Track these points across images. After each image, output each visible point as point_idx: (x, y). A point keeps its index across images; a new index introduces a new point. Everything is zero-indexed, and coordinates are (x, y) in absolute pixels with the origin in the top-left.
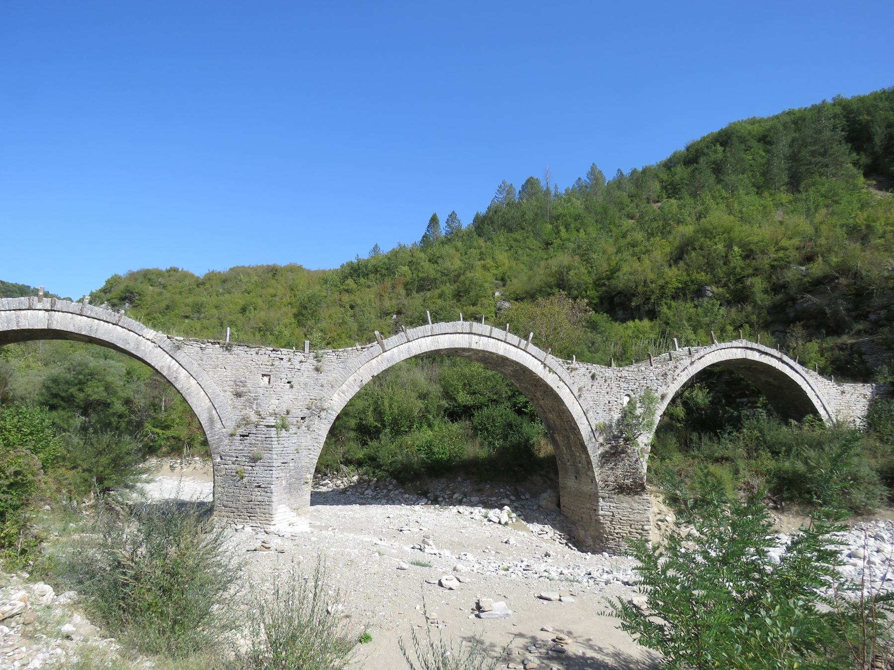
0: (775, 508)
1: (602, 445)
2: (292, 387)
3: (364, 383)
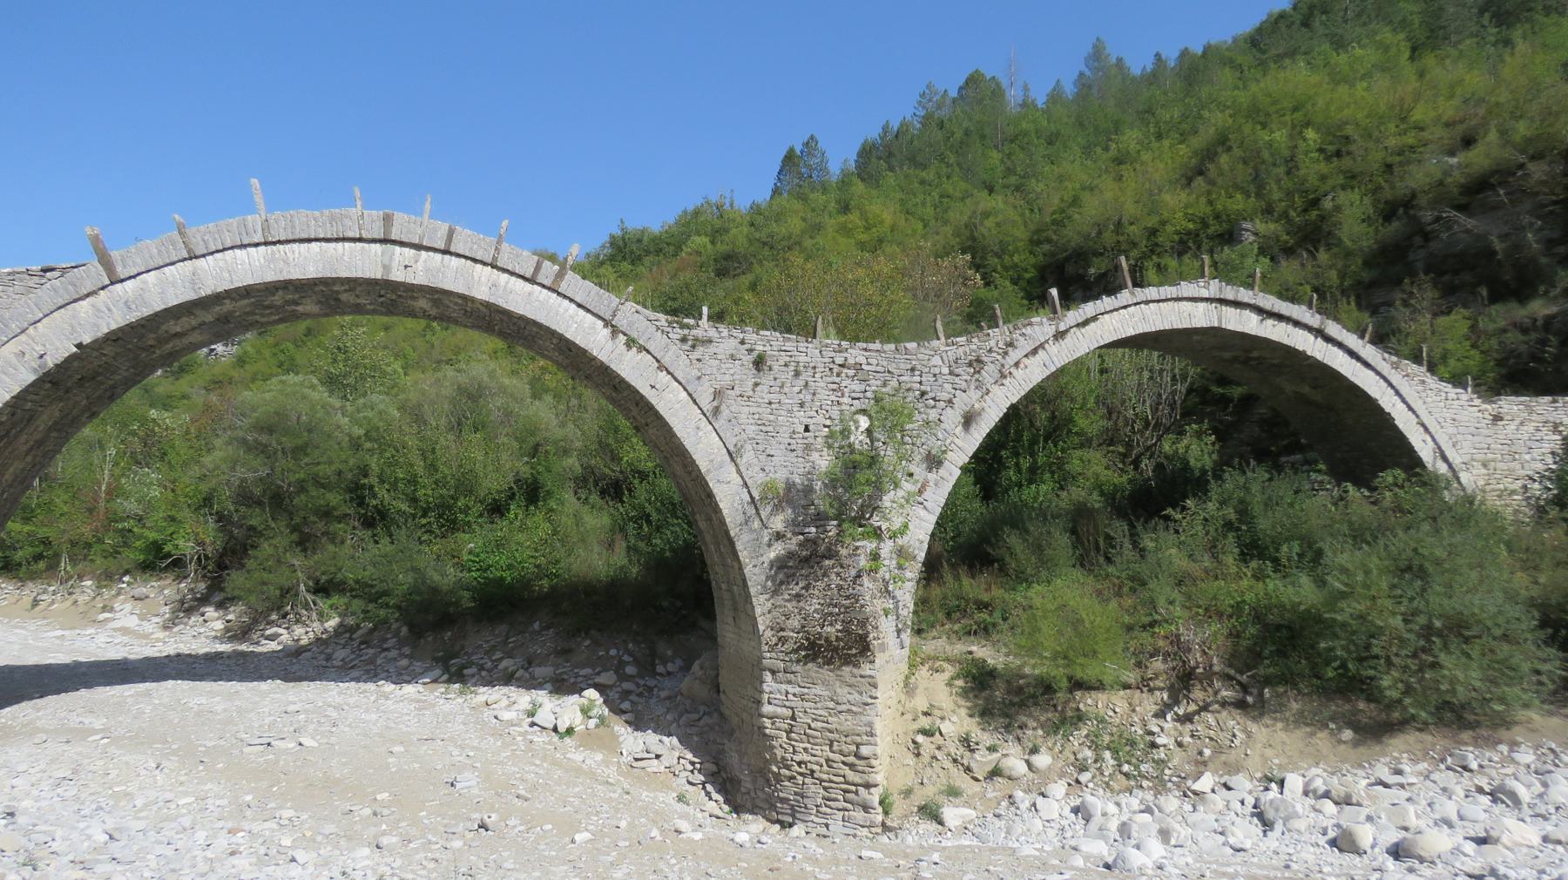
0: (1241, 705)
1: (779, 536)
3: (50, 362)
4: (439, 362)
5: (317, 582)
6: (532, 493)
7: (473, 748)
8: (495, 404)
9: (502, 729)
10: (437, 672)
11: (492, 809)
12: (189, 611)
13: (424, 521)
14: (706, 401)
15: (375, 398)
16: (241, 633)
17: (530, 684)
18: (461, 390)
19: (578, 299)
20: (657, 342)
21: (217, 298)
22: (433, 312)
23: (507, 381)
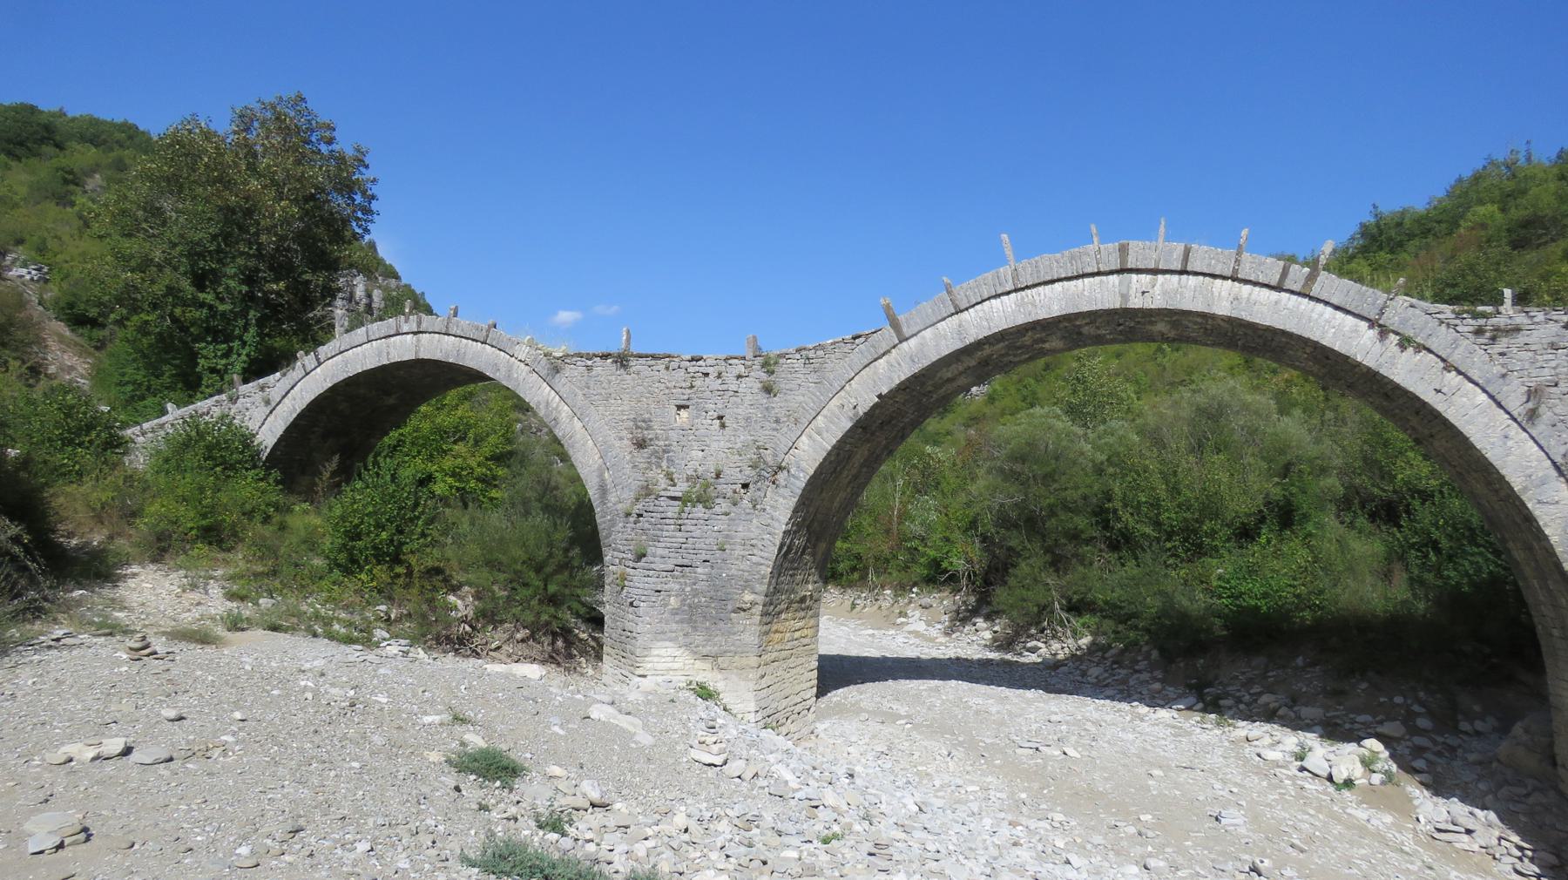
2: (723, 426)
3: (861, 411)
4: (1172, 384)
5: (1069, 600)
6: (1286, 516)
7: (1236, 784)
8: (1237, 423)
9: (1268, 770)
10: (1192, 700)
11: (1263, 854)
12: (964, 621)
13: (1169, 545)
14: (1516, 403)
15: (1113, 424)
16: (1005, 644)
17: (1297, 724)
18: (1200, 410)
19: (1335, 301)
20: (1441, 339)
21: (979, 345)
22: (1172, 334)
23: (1249, 398)
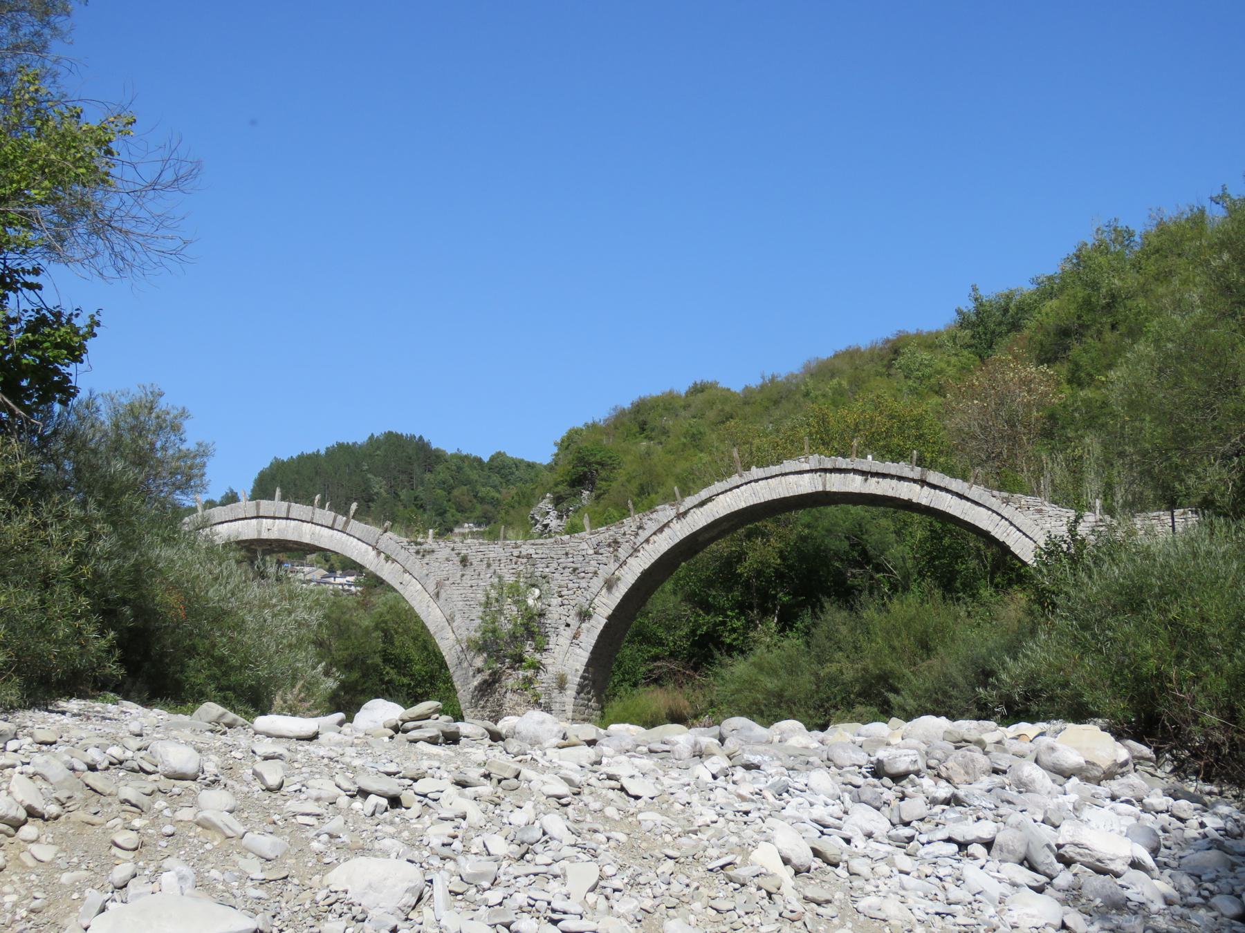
14: (432, 588)
